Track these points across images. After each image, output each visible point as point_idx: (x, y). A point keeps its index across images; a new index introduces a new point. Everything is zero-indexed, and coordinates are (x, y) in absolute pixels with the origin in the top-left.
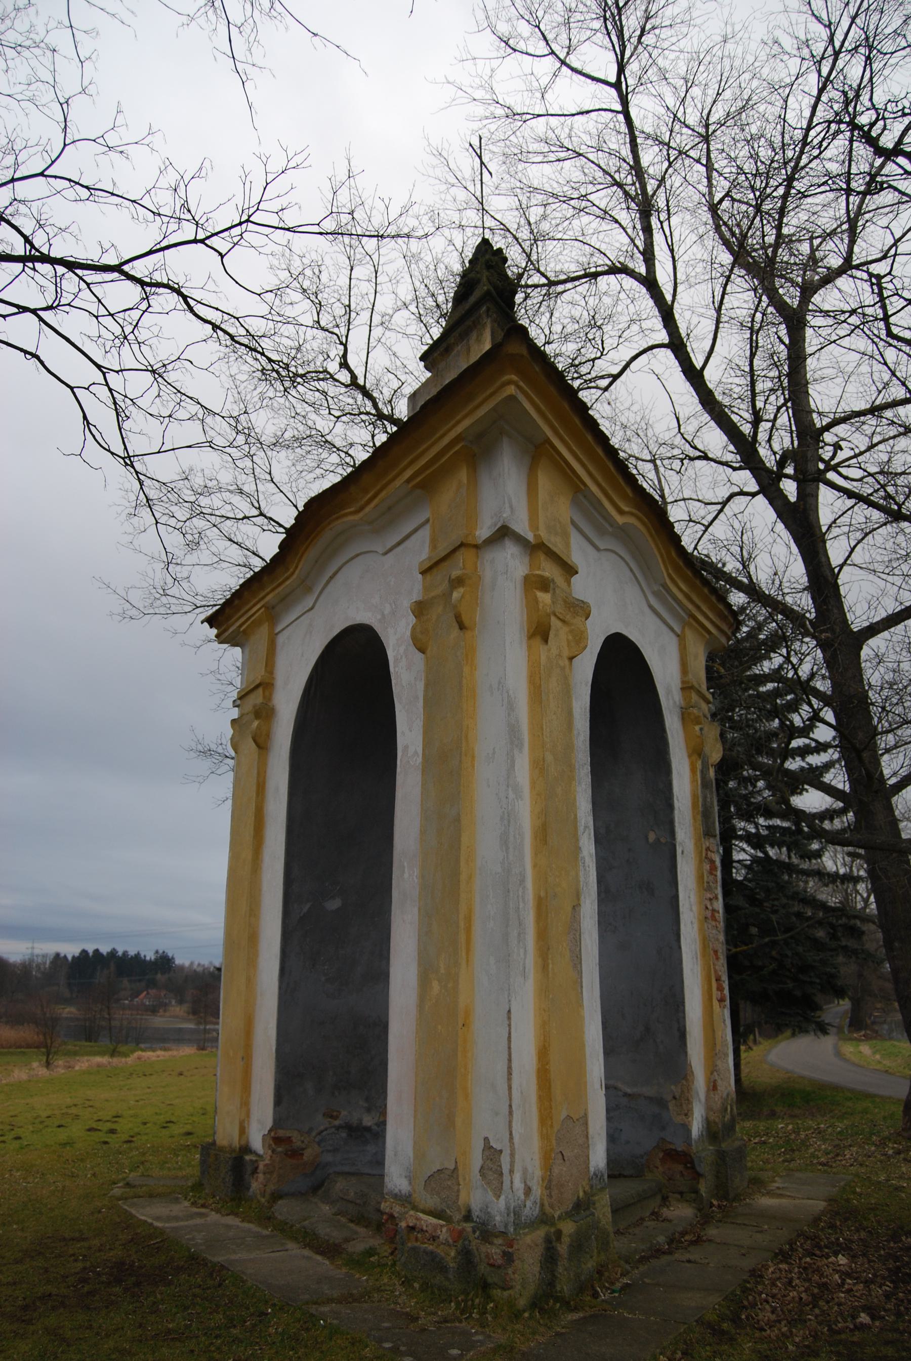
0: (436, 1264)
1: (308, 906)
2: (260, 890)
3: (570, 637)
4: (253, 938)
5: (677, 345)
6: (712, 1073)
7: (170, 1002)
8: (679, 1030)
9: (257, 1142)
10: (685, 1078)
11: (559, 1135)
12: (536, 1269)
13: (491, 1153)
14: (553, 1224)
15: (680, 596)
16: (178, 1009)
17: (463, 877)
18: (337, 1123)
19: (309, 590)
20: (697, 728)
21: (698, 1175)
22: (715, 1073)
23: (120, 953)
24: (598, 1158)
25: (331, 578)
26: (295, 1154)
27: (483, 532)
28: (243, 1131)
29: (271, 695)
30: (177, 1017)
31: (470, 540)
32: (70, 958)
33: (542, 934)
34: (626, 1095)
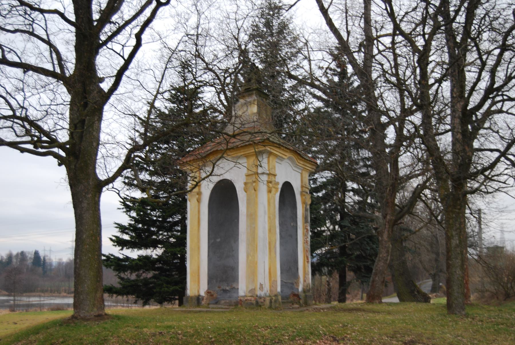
0: (252, 304)
9: (203, 293)
11: (273, 283)
15: (301, 165)
21: (300, 299)
24: (279, 289)
26: (212, 295)
33: (270, 248)
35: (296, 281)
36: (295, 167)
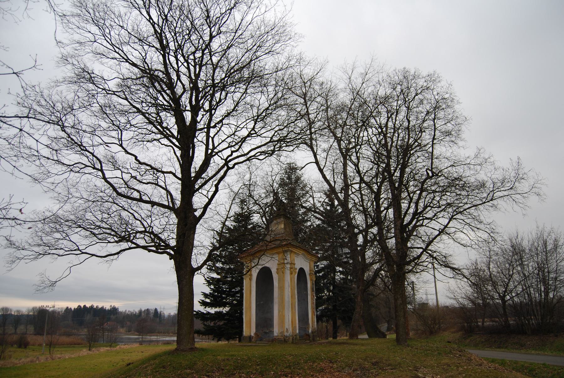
0: (282, 341)
5: (317, 163)
9: (252, 334)
13: (287, 329)
23: (95, 307)
24: (297, 332)
26: (258, 336)
32: (73, 309)
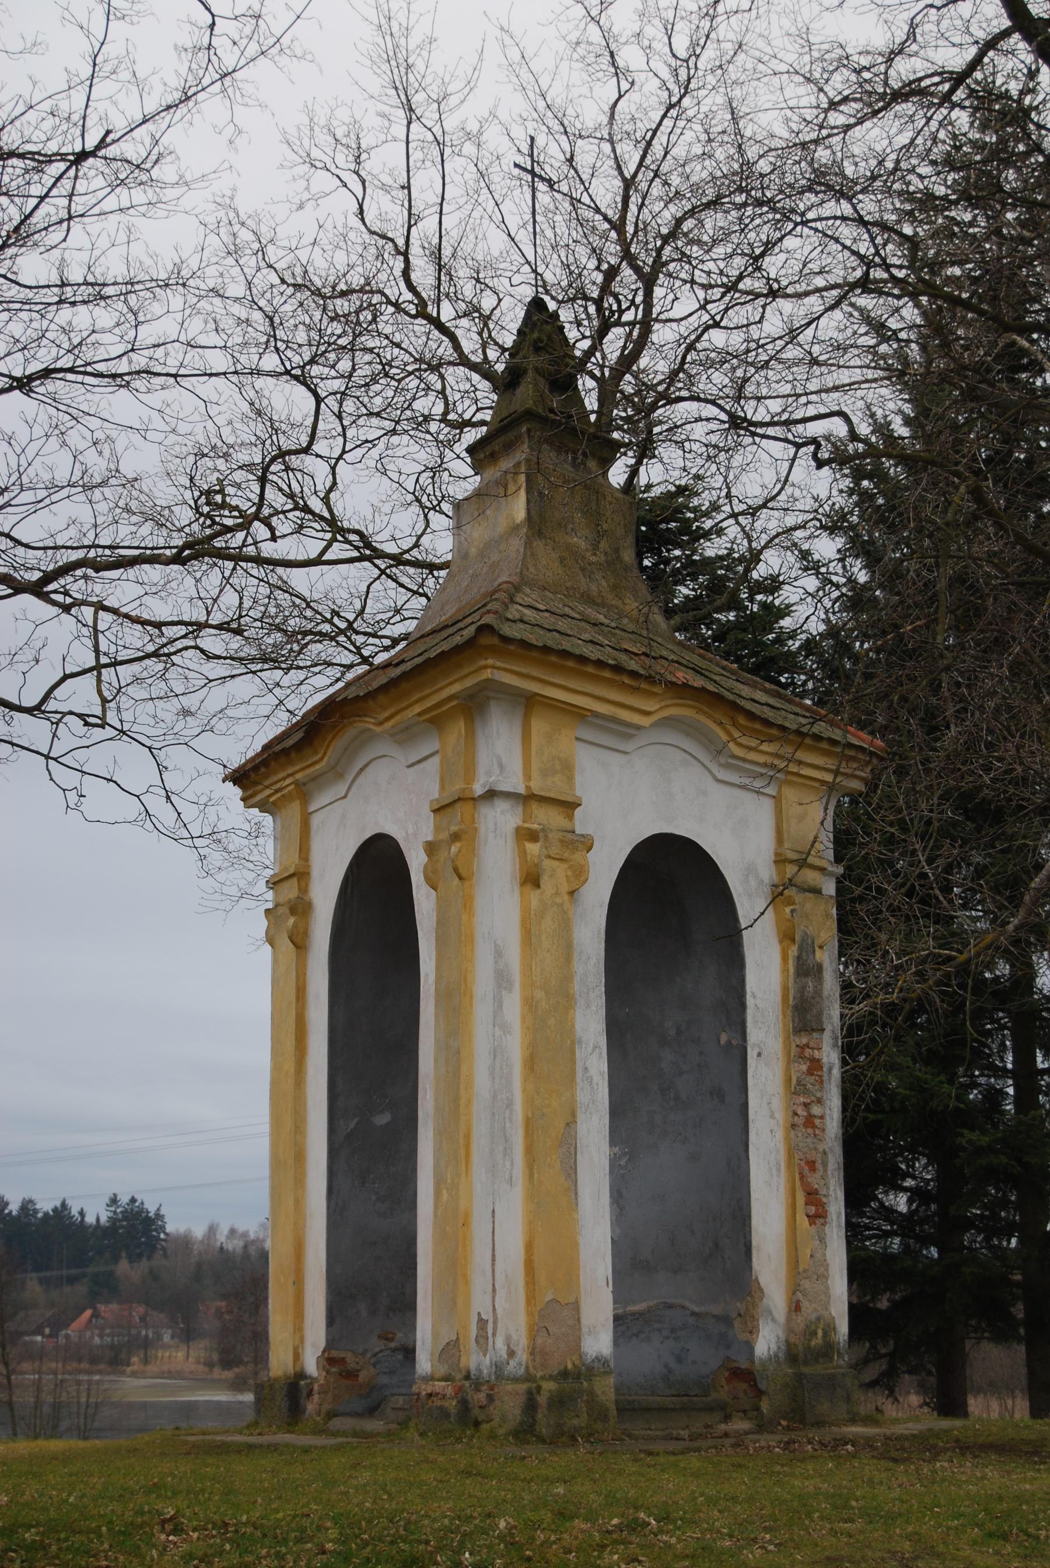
0: (444, 1413)
1: (356, 1120)
2: (305, 1105)
3: (569, 873)
4: (300, 1157)
6: (794, 1293)
7: (159, 1337)
8: (745, 1245)
9: (311, 1366)
10: (750, 1294)
11: (554, 1314)
12: (518, 1411)
13: (482, 1323)
14: (535, 1381)
16: (181, 1355)
17: (463, 1102)
18: (393, 1345)
19: (341, 776)
20: (788, 910)
22: (799, 1294)
24: (599, 1341)
25: (362, 769)
26: (350, 1375)
27: (478, 789)
28: (297, 1356)
29: (307, 885)
30: (178, 1375)
31: (467, 794)
34: (693, 1314)
35: (741, 1306)
36: (727, 766)
